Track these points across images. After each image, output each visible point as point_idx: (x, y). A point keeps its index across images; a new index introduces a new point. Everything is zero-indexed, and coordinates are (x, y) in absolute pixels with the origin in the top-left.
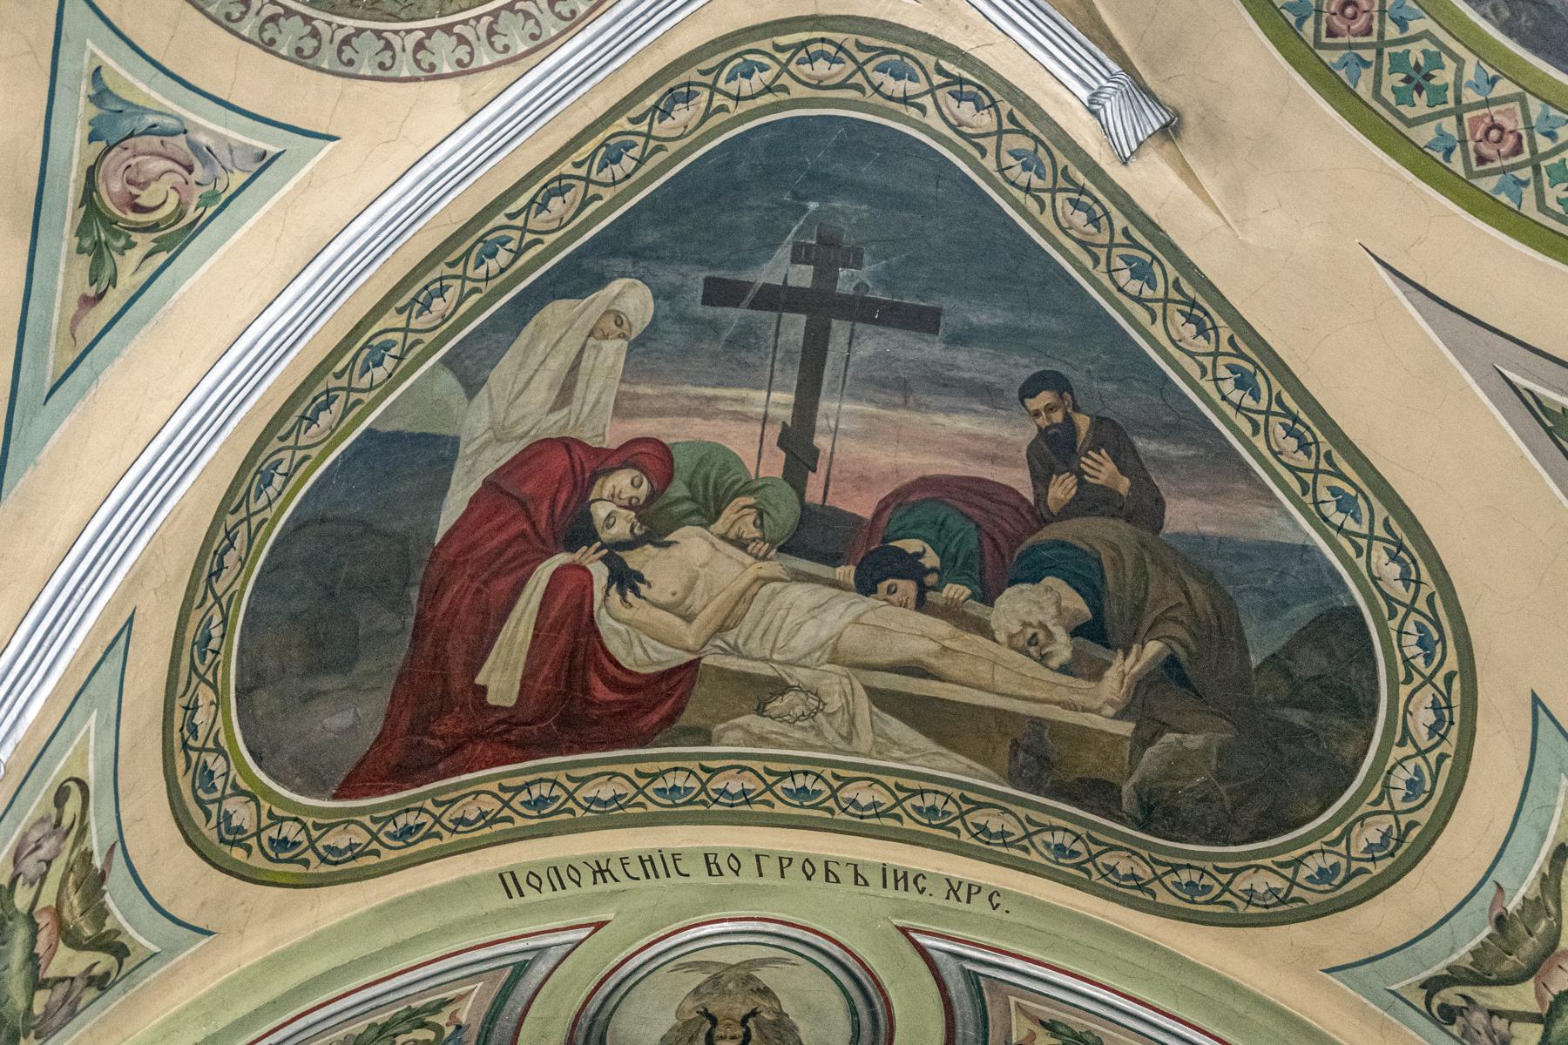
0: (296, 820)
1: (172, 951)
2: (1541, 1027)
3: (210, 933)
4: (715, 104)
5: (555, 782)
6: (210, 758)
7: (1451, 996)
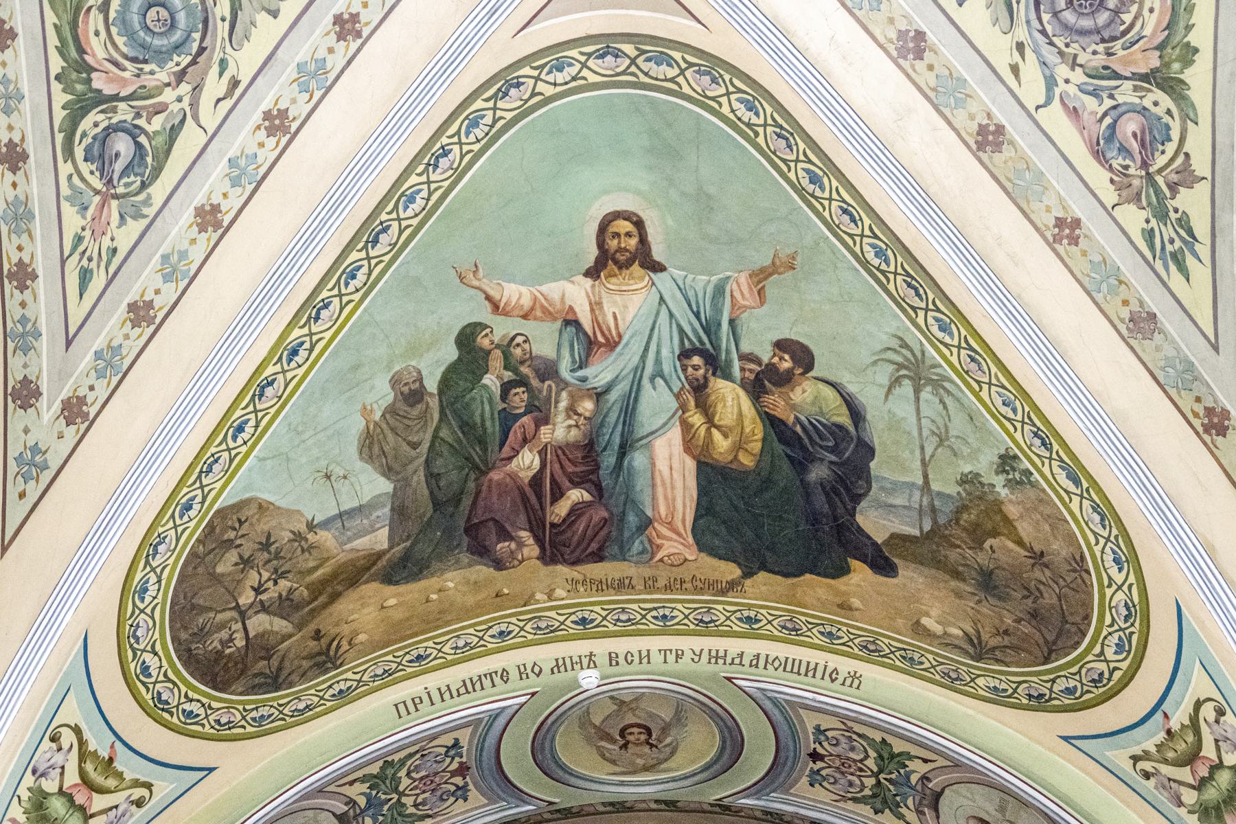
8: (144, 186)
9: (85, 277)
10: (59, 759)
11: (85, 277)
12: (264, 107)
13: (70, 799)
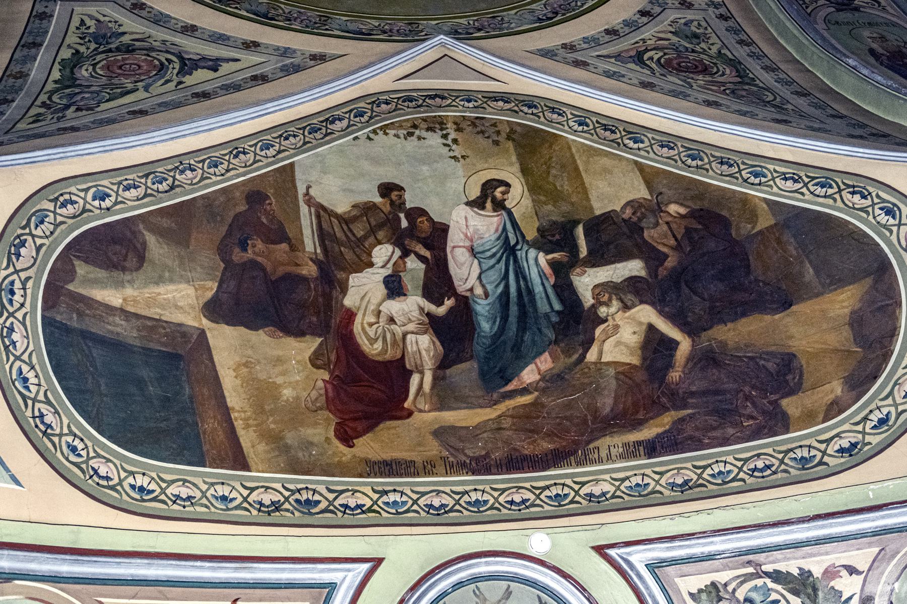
3: (17, 482)
5: (402, 493)
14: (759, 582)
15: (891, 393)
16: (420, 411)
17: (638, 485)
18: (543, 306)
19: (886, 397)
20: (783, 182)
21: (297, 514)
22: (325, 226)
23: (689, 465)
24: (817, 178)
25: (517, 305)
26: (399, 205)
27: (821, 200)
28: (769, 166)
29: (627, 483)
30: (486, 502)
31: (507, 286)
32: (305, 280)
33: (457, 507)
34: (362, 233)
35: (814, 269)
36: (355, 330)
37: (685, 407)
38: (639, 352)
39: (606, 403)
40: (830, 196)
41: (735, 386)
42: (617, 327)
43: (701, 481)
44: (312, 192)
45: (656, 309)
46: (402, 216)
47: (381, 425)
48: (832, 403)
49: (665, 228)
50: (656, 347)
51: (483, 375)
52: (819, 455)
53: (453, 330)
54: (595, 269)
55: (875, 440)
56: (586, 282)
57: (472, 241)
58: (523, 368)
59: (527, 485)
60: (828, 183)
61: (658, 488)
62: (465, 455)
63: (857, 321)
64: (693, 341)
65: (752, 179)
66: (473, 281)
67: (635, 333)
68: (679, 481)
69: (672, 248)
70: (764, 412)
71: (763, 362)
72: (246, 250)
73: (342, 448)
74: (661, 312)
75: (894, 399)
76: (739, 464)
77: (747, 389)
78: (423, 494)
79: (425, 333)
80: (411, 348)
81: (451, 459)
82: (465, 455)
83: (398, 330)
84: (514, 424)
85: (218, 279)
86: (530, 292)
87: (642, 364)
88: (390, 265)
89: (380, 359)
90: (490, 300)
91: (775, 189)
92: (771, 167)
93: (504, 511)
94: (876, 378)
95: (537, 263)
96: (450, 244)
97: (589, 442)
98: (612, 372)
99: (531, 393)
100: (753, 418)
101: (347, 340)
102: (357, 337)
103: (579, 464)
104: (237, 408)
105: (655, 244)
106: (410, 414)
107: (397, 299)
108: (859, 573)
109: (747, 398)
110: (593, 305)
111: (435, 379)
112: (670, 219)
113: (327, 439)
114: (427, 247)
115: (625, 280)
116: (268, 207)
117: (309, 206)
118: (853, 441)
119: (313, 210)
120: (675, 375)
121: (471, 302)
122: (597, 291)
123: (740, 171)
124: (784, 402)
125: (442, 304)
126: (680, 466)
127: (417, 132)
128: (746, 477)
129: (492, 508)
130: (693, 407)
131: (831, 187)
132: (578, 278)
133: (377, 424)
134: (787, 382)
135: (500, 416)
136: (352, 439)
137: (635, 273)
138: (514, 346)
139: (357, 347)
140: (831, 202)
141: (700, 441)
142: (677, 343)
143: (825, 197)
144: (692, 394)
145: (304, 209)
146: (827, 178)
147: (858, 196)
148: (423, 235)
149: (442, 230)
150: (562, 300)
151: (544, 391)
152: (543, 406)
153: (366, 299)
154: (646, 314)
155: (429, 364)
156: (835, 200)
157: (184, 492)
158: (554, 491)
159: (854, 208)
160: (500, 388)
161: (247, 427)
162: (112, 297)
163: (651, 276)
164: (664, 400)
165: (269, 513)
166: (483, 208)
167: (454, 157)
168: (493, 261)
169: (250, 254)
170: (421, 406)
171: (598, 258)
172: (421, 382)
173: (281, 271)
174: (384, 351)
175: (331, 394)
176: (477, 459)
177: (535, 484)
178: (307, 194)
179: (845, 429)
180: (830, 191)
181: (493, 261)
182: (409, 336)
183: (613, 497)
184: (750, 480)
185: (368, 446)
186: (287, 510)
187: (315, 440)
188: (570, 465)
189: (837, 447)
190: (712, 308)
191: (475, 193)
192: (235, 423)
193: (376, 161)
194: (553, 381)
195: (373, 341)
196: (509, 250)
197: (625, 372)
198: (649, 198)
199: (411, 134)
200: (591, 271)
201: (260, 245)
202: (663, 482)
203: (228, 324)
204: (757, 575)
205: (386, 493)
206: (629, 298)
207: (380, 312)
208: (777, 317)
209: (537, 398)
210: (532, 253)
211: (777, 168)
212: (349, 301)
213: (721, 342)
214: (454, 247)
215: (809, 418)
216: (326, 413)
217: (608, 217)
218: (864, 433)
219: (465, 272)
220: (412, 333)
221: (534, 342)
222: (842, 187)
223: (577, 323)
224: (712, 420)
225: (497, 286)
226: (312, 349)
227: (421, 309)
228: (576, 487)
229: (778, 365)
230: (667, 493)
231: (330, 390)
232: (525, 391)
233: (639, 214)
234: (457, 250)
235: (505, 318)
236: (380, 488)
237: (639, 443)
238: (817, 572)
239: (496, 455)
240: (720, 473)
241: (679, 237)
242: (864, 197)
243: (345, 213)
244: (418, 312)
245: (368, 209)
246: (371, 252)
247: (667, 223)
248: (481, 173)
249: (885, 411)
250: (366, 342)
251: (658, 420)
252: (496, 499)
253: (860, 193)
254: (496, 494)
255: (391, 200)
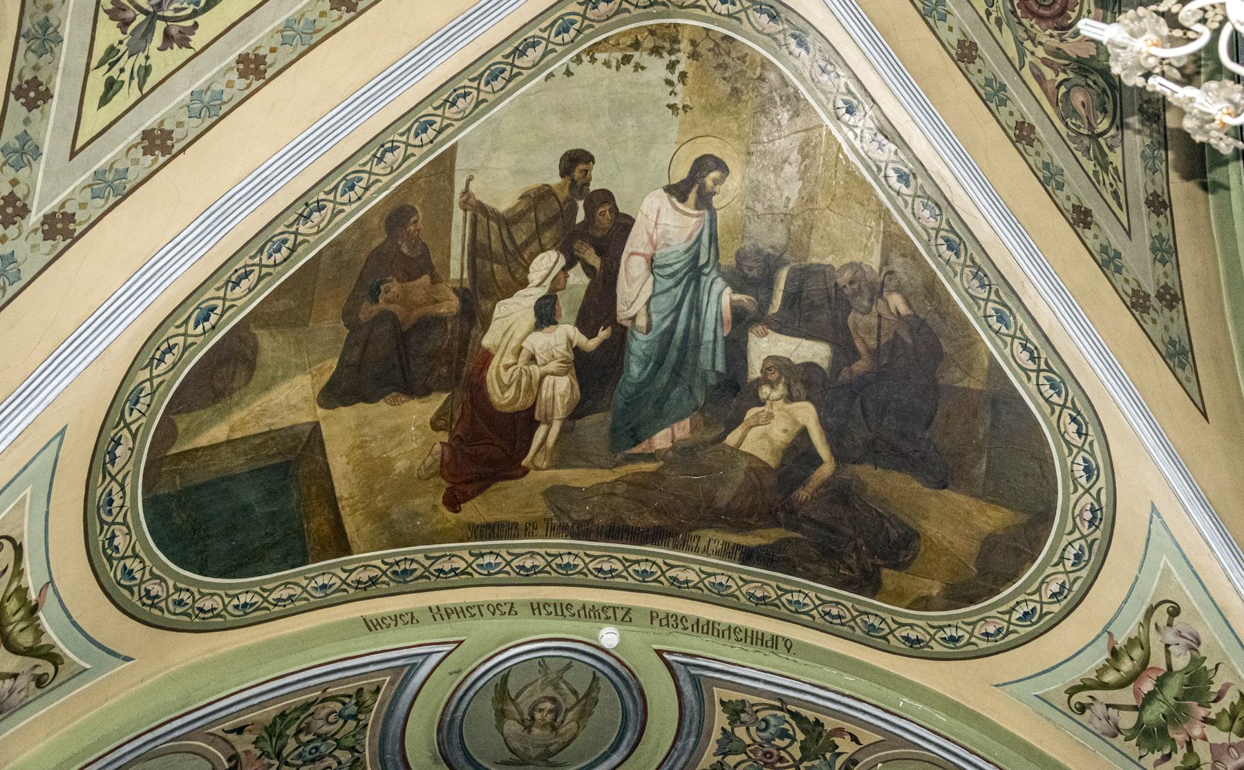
0: (188, 590)
1: (99, 670)
2: (1136, 714)
3: (127, 659)
4: (223, 290)
5: (498, 555)
6: (128, 562)
7: (1082, 697)
8: (195, 14)
9: (111, 87)
10: (1099, 709)
11: (111, 87)
12: (54, 103)
13: (1150, 698)
14: (780, 714)
15: (974, 624)
16: (537, 469)
17: (721, 584)
18: (705, 358)
19: (969, 624)
20: (1020, 349)
21: (392, 584)
22: (481, 236)
23: (774, 584)
24: (1054, 373)
25: (677, 350)
26: (578, 188)
27: (1041, 401)
28: (1018, 317)
29: (712, 579)
30: (576, 566)
31: (675, 321)
32: (441, 320)
33: (548, 569)
34: (524, 237)
35: (988, 466)
36: (488, 376)
37: (796, 529)
38: (780, 455)
39: (724, 495)
40: (1051, 404)
41: (852, 533)
42: (770, 416)
43: (777, 602)
44: (473, 188)
45: (819, 413)
46: (581, 203)
47: (493, 487)
48: (924, 598)
49: (874, 321)
50: (799, 452)
51: (613, 430)
52: (887, 630)
53: (595, 372)
54: (778, 335)
55: (938, 648)
56: (765, 346)
57: (655, 248)
58: (658, 430)
59: (620, 556)
60: (1058, 387)
61: (738, 593)
62: (570, 518)
63: (990, 544)
64: (837, 468)
65: (992, 321)
66: (639, 306)
67: (785, 431)
68: (759, 594)
69: (869, 351)
70: (863, 570)
71: (888, 525)
72: (377, 301)
73: (449, 514)
74: (822, 421)
75: (973, 629)
76: (817, 602)
77: (860, 541)
78: (518, 556)
79: (566, 374)
80: (545, 393)
81: (555, 521)
82: (570, 518)
83: (536, 370)
84: (627, 491)
85: (340, 351)
86: (698, 336)
87: (777, 469)
88: (548, 283)
89: (508, 410)
90: (651, 336)
91: (1007, 351)
92: (1020, 320)
93: (591, 577)
94: (972, 602)
95: (721, 298)
96: (628, 248)
97: (695, 529)
98: (744, 464)
99: (656, 461)
100: (850, 569)
101: (477, 389)
102: (489, 384)
103: (675, 547)
104: (346, 496)
105: (854, 335)
106: (526, 471)
107: (546, 329)
108: (858, 743)
109: (856, 549)
110: (758, 380)
111: (563, 431)
112: (885, 313)
113: (435, 507)
114: (600, 252)
115: (803, 364)
116: (412, 228)
117: (465, 210)
118: (920, 637)
119: (469, 213)
120: (803, 494)
121: (629, 334)
122: (770, 364)
123: (987, 300)
124: (885, 571)
125: (595, 335)
126: (765, 582)
127: (637, 55)
128: (817, 616)
129: (580, 572)
130: (803, 533)
131: (1059, 394)
132: (756, 339)
133: (488, 486)
134: (898, 555)
135: (616, 481)
136: (460, 503)
137: (817, 360)
138: (658, 402)
139: (486, 398)
140: (1048, 410)
141: (794, 567)
142: (821, 462)
143: (1047, 400)
144: (810, 520)
145: (458, 215)
146: (1062, 381)
147: (1076, 427)
148: (599, 234)
149: (624, 225)
150: (729, 360)
151: (669, 463)
152: (664, 479)
153: (509, 334)
154: (806, 413)
155: (560, 412)
156: (1053, 412)
157: (285, 594)
158: (643, 566)
159: (1063, 436)
160: (627, 448)
161: (353, 513)
162: (218, 433)
163: (831, 372)
164: (781, 515)
165: (365, 589)
166: (683, 199)
167: (672, 107)
168: (670, 282)
169: (382, 304)
170: (538, 464)
171: (783, 326)
172: (546, 435)
173: (417, 314)
174: (515, 399)
175: (447, 458)
176: (579, 524)
177: (628, 556)
178: (466, 191)
179: (919, 623)
180: (1055, 399)
181: (670, 282)
182: (547, 378)
183: (695, 587)
184: (819, 620)
185: (475, 510)
186: (384, 583)
187: (421, 510)
188: (666, 546)
189: (905, 634)
190: (873, 442)
191: (681, 173)
192: (342, 512)
193: (566, 114)
194: (683, 453)
195: (504, 388)
196: (694, 272)
197: (757, 468)
198: (877, 270)
199: (626, 59)
200: (773, 336)
201: (395, 287)
202: (744, 589)
203: (345, 405)
204: (781, 709)
205: (482, 555)
206: (799, 388)
207: (522, 348)
208: (927, 490)
209: (662, 467)
210: (720, 283)
211: (1025, 328)
212: (487, 341)
213: (862, 483)
214: (632, 254)
215: (897, 597)
216: (438, 479)
217: (822, 271)
218: (933, 637)
219: (635, 291)
220: (552, 374)
221: (680, 400)
222: (1069, 404)
223: (733, 393)
224: (813, 552)
225: (665, 318)
226: (437, 407)
227: (570, 341)
228: (665, 568)
229: (900, 535)
230: (743, 600)
231: (446, 453)
232: (651, 457)
233: (855, 286)
234: (634, 258)
235: (659, 363)
236: (477, 552)
237: (738, 546)
238: (828, 728)
239: (601, 521)
240: (798, 602)
241: (884, 341)
242: (1079, 433)
243: (509, 210)
244: (564, 346)
245: (543, 194)
246: (529, 265)
247: (880, 316)
248: (699, 140)
249: (960, 633)
250: (498, 390)
251: (764, 532)
252: (586, 565)
253: (1080, 425)
254: (587, 560)
255: (573, 181)
